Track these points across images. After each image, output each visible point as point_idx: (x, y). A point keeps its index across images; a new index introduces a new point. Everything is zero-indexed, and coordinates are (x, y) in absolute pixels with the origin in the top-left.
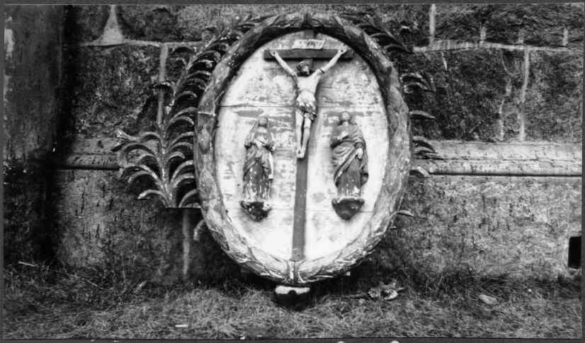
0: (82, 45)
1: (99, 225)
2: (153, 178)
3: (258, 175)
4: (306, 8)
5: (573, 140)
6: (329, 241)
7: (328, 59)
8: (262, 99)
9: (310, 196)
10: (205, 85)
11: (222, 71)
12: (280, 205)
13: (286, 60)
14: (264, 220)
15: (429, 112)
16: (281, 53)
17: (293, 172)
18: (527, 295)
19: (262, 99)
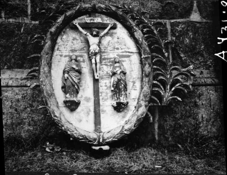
0: (211, 21)
1: (202, 115)
2: (174, 90)
3: (71, 88)
4: (168, 1)
5: (109, 70)
6: (82, 122)
7: (105, 28)
8: (118, 49)
9: (92, 99)
10: (147, 42)
11: (138, 34)
12: (87, 105)
13: (83, 28)
14: (116, 112)
15: (146, 55)
16: (79, 24)
17: (101, 86)
18: (159, 147)
19: (118, 49)
